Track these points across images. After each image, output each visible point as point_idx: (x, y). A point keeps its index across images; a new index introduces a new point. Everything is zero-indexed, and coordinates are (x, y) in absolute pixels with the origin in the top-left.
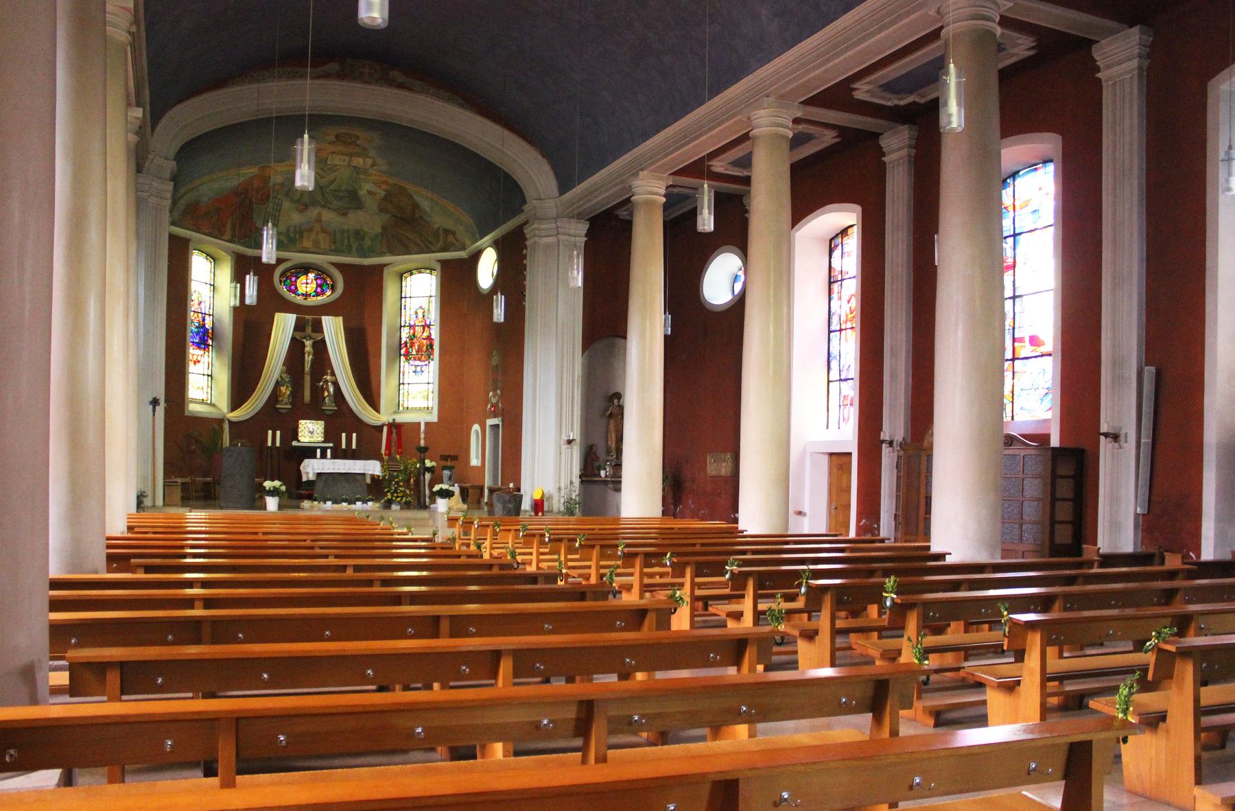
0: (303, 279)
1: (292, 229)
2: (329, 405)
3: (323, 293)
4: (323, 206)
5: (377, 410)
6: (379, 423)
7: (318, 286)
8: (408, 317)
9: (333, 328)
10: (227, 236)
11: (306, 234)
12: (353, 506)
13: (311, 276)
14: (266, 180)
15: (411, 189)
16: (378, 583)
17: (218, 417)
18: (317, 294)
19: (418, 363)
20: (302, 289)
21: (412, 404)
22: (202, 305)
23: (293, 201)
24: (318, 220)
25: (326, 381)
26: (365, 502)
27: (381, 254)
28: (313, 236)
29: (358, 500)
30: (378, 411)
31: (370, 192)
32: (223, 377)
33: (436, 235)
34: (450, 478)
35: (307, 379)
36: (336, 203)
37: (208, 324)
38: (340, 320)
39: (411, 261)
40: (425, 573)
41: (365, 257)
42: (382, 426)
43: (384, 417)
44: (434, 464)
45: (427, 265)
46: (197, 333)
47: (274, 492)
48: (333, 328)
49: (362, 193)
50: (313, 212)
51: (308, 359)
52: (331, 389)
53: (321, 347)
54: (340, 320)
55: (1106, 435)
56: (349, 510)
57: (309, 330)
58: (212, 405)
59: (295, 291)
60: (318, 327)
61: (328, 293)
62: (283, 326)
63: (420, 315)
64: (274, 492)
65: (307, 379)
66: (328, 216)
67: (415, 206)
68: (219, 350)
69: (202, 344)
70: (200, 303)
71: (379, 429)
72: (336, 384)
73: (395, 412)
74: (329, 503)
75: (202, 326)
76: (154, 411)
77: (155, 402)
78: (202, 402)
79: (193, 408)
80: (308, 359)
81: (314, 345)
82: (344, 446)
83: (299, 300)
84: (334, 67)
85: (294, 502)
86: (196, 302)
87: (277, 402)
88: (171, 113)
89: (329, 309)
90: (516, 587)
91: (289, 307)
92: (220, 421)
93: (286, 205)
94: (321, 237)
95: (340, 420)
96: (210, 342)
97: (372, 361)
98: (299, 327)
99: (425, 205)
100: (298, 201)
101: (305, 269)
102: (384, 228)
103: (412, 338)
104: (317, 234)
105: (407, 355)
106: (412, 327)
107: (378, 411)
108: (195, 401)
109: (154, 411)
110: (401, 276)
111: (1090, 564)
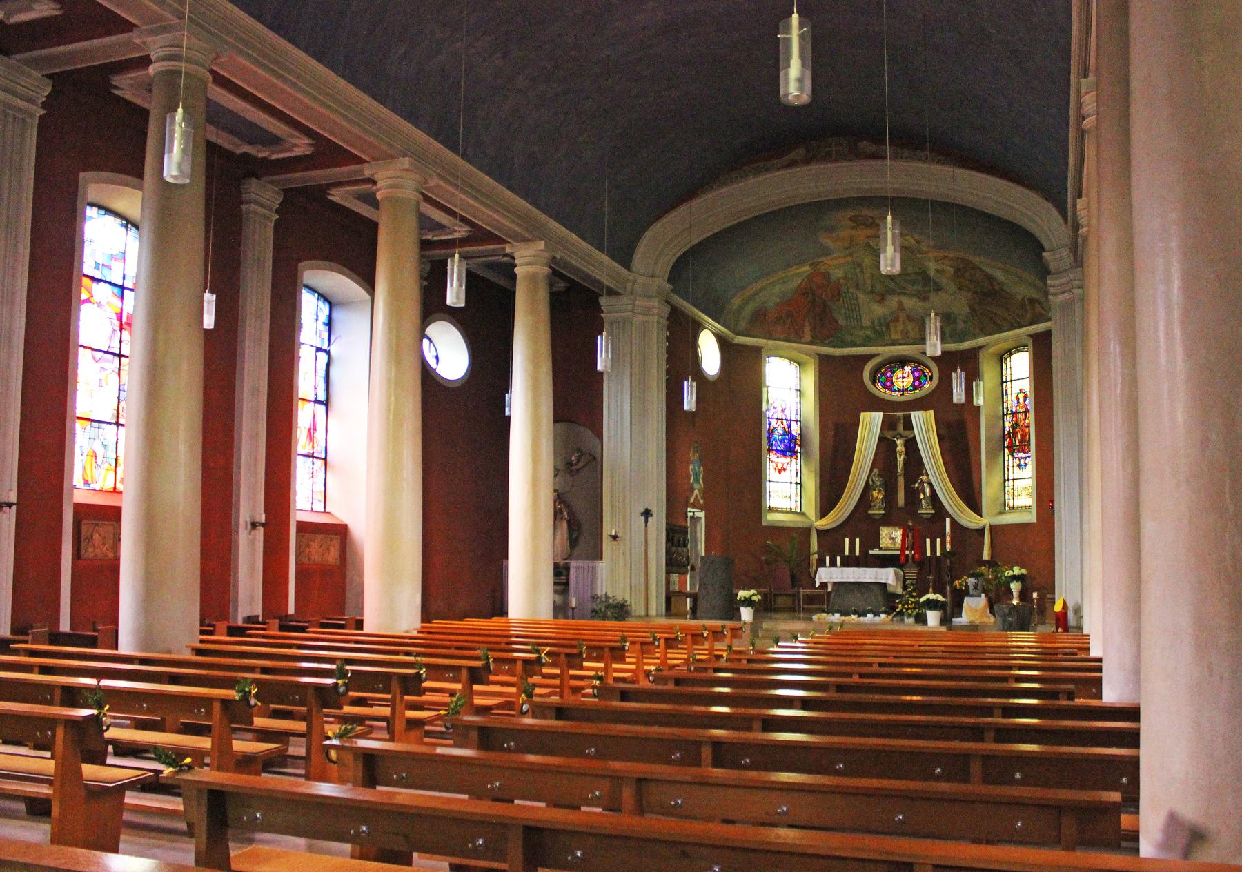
0: (899, 373)
1: (876, 322)
2: (926, 510)
3: (921, 386)
4: (900, 294)
5: (978, 512)
6: (979, 526)
7: (915, 379)
8: (1010, 403)
9: (923, 423)
10: (808, 337)
11: (892, 325)
12: (862, 619)
13: (907, 369)
14: (826, 276)
15: (977, 260)
16: (999, 712)
17: (805, 526)
18: (915, 388)
19: (1021, 455)
20: (898, 384)
21: (1019, 502)
22: (787, 412)
23: (865, 292)
24: (901, 307)
25: (922, 482)
26: (876, 614)
27: (975, 336)
28: (900, 327)
29: (869, 612)
30: (979, 513)
31: (937, 271)
32: (811, 484)
33: (1022, 306)
34: (976, 587)
35: (901, 480)
36: (910, 288)
37: (795, 430)
38: (931, 414)
39: (1003, 340)
40: (1034, 701)
41: (962, 341)
42: (983, 530)
43: (986, 521)
44: (1024, 571)
45: (1023, 342)
46: (781, 441)
47: (748, 602)
48: (923, 423)
49: (932, 273)
50: (893, 301)
51: (900, 459)
52: (927, 491)
53: (911, 444)
54: (931, 414)
55: (10, 505)
56: (859, 624)
57: (901, 428)
58: (802, 514)
59: (891, 388)
60: (908, 425)
61: (927, 386)
62: (871, 424)
63: (1021, 401)
64: (748, 602)
65: (901, 480)
66: (909, 303)
67: (991, 279)
68: (806, 455)
69: (789, 451)
70: (783, 410)
71: (981, 532)
72: (930, 484)
73: (1001, 513)
74: (870, 616)
75: (788, 432)
76: (646, 522)
77: (647, 513)
78: (791, 511)
79: (772, 518)
80: (900, 459)
81: (906, 444)
82: (928, 554)
83: (895, 396)
84: (800, 152)
85: (807, 615)
86: (780, 409)
87: (870, 507)
88: (648, 235)
89: (920, 404)
90: (904, 698)
91: (876, 404)
92: (806, 532)
93: (861, 297)
94: (910, 327)
95: (923, 521)
96: (798, 448)
97: (973, 459)
98: (888, 424)
99: (1000, 275)
100: (872, 292)
101: (901, 362)
102: (970, 307)
103: (1014, 426)
104: (904, 323)
105: (1011, 447)
106: (1014, 414)
107: (979, 513)
108: (771, 510)
109: (646, 522)
110: (1001, 358)
111: (805, 633)
